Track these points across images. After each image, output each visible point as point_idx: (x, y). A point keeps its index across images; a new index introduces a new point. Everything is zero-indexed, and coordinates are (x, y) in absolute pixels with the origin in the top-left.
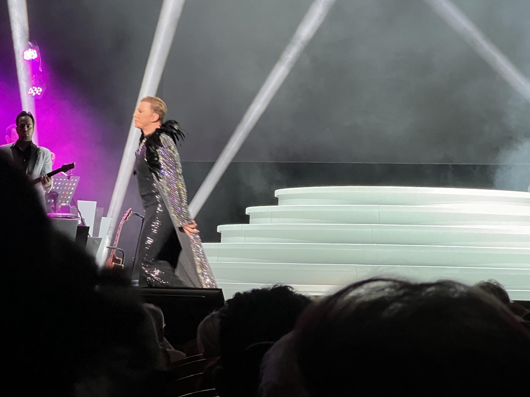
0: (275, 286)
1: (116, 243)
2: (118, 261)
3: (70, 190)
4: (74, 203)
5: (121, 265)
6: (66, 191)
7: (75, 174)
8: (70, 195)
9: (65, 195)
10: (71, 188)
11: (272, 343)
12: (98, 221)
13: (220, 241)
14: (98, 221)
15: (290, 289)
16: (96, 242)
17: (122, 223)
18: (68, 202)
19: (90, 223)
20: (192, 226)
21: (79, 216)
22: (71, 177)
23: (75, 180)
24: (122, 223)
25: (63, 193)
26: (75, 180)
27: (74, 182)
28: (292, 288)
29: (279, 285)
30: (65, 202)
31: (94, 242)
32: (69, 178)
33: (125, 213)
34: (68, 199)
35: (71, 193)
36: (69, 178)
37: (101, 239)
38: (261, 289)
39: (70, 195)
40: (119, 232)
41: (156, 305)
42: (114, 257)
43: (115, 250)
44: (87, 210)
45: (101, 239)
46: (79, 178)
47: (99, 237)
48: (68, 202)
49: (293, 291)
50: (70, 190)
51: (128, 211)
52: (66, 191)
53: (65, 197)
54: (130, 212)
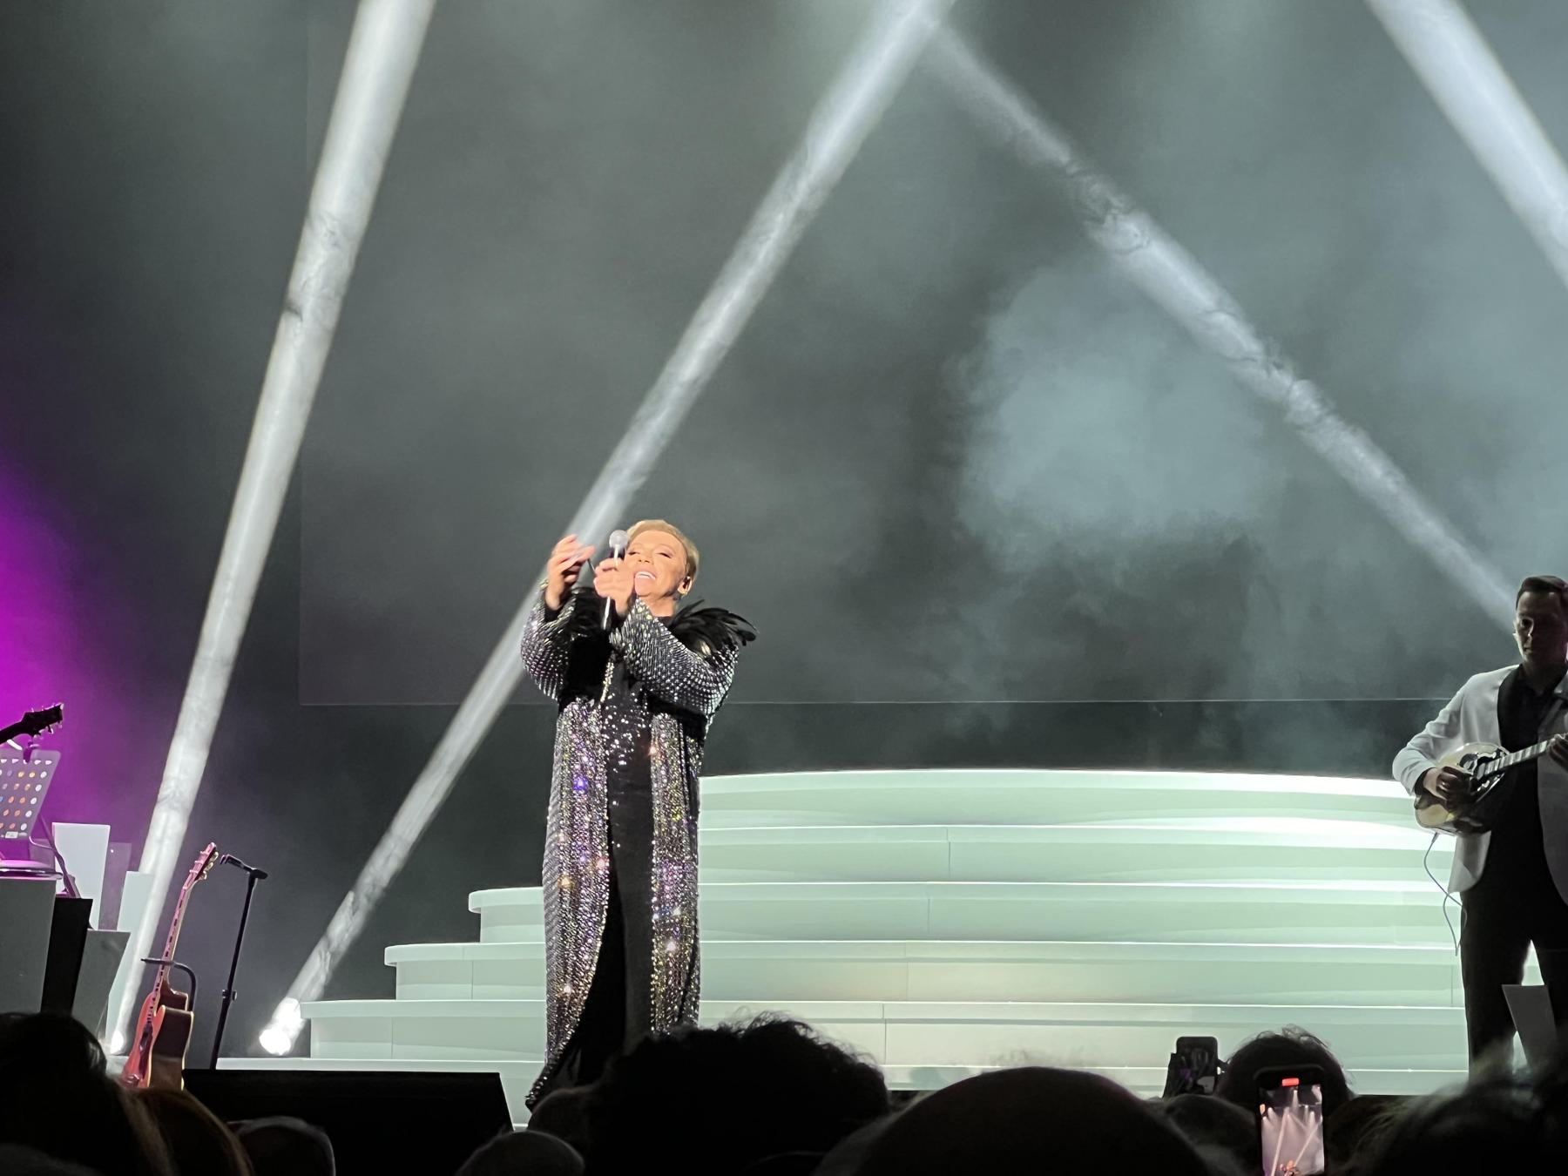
0: (758, 1020)
1: (171, 948)
2: (179, 1002)
3: (32, 793)
4: (42, 829)
5: (185, 1011)
6: (26, 780)
7: (46, 746)
8: (31, 807)
9: (13, 807)
10: (28, 801)
11: (1175, 1127)
12: (114, 883)
13: (476, 938)
14: (114, 883)
15: (802, 1032)
16: (113, 944)
17: (187, 887)
18: (24, 827)
19: (89, 887)
20: (740, 625)
21: (58, 869)
22: (35, 753)
23: (46, 763)
24: (187, 887)
25: (11, 800)
26: (46, 763)
27: (42, 767)
28: (805, 1026)
29: (770, 1019)
30: (17, 829)
31: (105, 946)
32: (27, 755)
33: (198, 856)
34: (27, 820)
35: (34, 801)
36: (27, 755)
37: (126, 936)
38: (715, 1028)
39: (31, 807)
40: (179, 914)
41: (308, 1121)
42: (165, 988)
43: (168, 968)
44: (81, 850)
45: (126, 936)
46: (57, 755)
47: (119, 930)
48: (24, 827)
49: (811, 1035)
50: (32, 793)
51: (207, 852)
52: (13, 807)
53: (17, 813)
54: (212, 854)
